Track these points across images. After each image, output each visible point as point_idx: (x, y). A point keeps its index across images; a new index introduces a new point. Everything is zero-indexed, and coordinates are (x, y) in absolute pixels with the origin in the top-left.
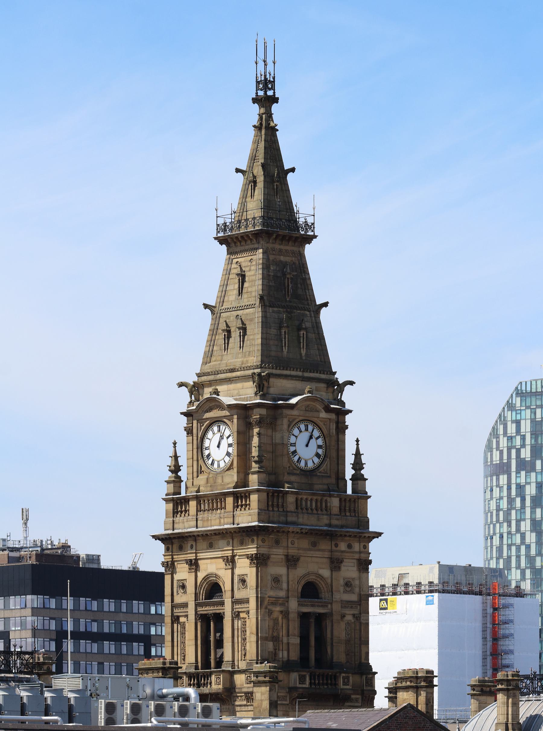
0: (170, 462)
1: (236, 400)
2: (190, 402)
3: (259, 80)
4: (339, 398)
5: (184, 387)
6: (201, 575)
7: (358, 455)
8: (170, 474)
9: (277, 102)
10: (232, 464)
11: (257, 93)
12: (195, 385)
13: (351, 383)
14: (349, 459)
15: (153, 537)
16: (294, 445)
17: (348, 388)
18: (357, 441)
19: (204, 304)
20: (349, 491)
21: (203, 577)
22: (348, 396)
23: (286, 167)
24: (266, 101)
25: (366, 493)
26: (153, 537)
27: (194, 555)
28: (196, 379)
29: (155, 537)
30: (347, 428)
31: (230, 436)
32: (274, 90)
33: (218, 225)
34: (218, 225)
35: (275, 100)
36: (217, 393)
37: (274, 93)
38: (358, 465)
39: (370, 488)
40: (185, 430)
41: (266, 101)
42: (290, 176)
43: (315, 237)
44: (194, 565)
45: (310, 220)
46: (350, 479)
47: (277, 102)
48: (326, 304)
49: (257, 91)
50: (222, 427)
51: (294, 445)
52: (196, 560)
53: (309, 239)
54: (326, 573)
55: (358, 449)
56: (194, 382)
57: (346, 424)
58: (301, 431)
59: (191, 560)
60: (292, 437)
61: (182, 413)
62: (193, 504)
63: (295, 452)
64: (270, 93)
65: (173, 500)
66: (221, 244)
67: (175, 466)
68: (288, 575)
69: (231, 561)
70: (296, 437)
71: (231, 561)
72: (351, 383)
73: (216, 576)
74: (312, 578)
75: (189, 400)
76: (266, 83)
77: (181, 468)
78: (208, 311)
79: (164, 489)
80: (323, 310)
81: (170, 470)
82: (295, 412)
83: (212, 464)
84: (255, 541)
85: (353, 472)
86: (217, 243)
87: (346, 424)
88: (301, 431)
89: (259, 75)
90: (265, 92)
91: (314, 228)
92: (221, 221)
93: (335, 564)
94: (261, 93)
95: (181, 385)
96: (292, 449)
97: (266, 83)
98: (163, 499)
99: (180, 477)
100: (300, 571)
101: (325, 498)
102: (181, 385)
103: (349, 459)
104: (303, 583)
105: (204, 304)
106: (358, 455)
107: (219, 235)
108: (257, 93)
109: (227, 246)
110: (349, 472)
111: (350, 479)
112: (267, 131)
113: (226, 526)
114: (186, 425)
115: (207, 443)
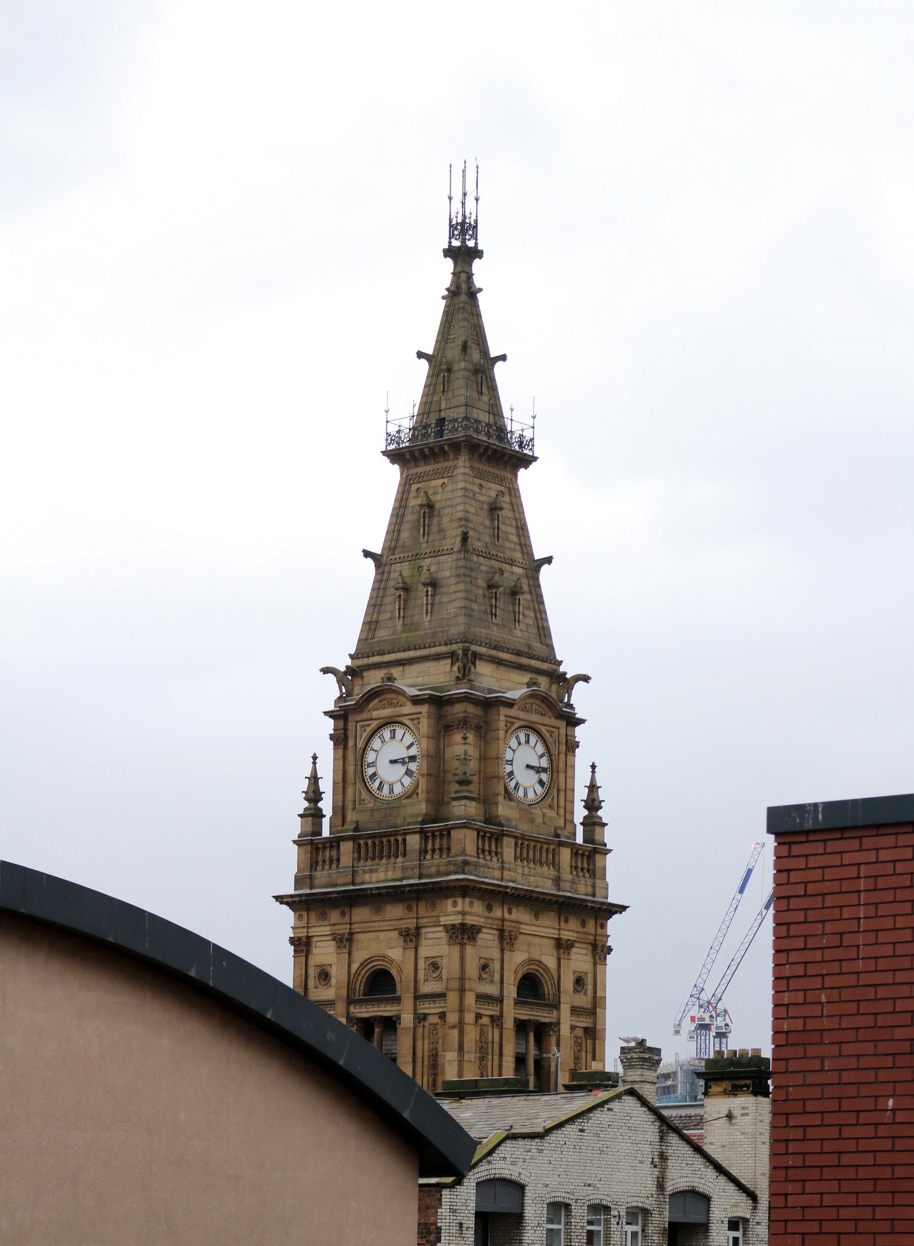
0: (305, 785)
1: (420, 690)
2: (341, 697)
3: (454, 222)
4: (566, 700)
5: (330, 676)
6: (360, 956)
7: (593, 788)
8: (306, 804)
9: (481, 257)
10: (417, 786)
11: (450, 243)
12: (350, 670)
13: (586, 679)
14: (581, 794)
15: (277, 898)
16: (511, 762)
17: (579, 686)
18: (593, 767)
19: (364, 551)
20: (579, 839)
21: (362, 961)
22: (581, 699)
23: (493, 354)
24: (463, 255)
25: (605, 845)
26: (277, 898)
27: (305, 930)
28: (349, 662)
29: (280, 899)
30: (578, 746)
31: (412, 744)
32: (476, 239)
33: (388, 434)
34: (388, 434)
35: (476, 253)
36: (390, 679)
37: (476, 244)
38: (593, 804)
39: (610, 837)
40: (331, 739)
41: (463, 255)
42: (499, 368)
43: (535, 459)
44: (345, 941)
45: (528, 434)
46: (581, 824)
47: (481, 257)
48: (549, 560)
49: (450, 238)
50: (400, 732)
51: (511, 762)
52: (309, 938)
53: (526, 461)
54: (550, 962)
55: (593, 778)
56: (347, 667)
57: (577, 739)
58: (520, 744)
59: (408, 929)
60: (508, 750)
61: (326, 713)
62: (347, 847)
63: (511, 774)
64: (471, 244)
65: (311, 842)
66: (393, 462)
67: (314, 792)
68: (502, 960)
69: (412, 937)
70: (514, 751)
71: (412, 937)
72: (586, 679)
73: (384, 958)
74: (379, 964)
75: (339, 695)
76: (464, 228)
77: (323, 796)
78: (370, 562)
79: (295, 827)
80: (545, 569)
81: (305, 799)
82: (513, 712)
83: (380, 787)
84: (414, 909)
85: (586, 813)
86: (386, 460)
87: (577, 739)
88: (520, 744)
89: (453, 216)
90: (464, 241)
91: (533, 445)
92: (393, 429)
93: (562, 946)
94: (456, 243)
95: (326, 671)
96: (508, 769)
97: (464, 228)
98: (294, 842)
99: (321, 810)
100: (518, 957)
101: (552, 847)
102: (326, 671)
103: (581, 794)
104: (520, 975)
105: (364, 551)
106: (593, 788)
107: (389, 448)
108: (450, 243)
109: (400, 467)
110: (580, 813)
111: (581, 824)
112: (462, 299)
113: (412, 881)
114: (332, 732)
115: (370, 757)
